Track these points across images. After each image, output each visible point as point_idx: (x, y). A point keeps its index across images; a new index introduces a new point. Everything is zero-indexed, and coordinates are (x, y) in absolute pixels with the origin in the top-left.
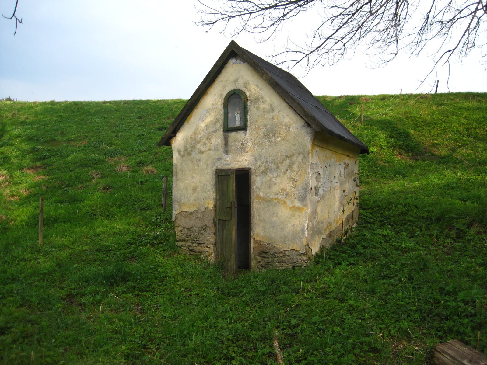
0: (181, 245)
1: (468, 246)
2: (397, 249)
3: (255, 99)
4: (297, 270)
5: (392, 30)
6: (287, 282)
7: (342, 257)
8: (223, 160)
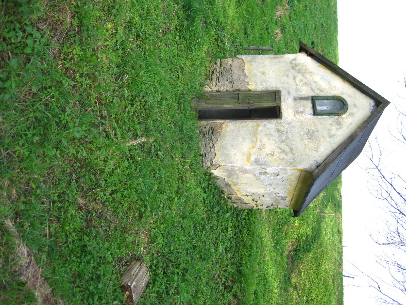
0: (217, 63)
1: (219, 294)
2: (216, 239)
3: (340, 122)
4: (199, 158)
5: (398, 240)
6: (190, 149)
7: (210, 194)
8: (288, 96)
